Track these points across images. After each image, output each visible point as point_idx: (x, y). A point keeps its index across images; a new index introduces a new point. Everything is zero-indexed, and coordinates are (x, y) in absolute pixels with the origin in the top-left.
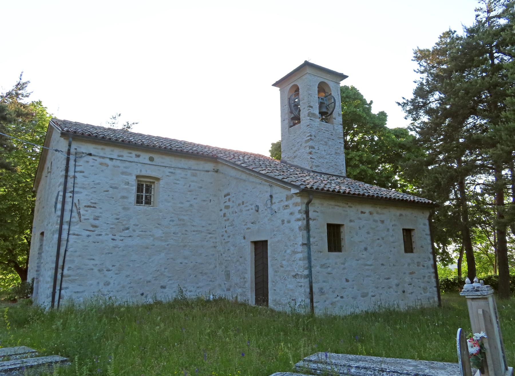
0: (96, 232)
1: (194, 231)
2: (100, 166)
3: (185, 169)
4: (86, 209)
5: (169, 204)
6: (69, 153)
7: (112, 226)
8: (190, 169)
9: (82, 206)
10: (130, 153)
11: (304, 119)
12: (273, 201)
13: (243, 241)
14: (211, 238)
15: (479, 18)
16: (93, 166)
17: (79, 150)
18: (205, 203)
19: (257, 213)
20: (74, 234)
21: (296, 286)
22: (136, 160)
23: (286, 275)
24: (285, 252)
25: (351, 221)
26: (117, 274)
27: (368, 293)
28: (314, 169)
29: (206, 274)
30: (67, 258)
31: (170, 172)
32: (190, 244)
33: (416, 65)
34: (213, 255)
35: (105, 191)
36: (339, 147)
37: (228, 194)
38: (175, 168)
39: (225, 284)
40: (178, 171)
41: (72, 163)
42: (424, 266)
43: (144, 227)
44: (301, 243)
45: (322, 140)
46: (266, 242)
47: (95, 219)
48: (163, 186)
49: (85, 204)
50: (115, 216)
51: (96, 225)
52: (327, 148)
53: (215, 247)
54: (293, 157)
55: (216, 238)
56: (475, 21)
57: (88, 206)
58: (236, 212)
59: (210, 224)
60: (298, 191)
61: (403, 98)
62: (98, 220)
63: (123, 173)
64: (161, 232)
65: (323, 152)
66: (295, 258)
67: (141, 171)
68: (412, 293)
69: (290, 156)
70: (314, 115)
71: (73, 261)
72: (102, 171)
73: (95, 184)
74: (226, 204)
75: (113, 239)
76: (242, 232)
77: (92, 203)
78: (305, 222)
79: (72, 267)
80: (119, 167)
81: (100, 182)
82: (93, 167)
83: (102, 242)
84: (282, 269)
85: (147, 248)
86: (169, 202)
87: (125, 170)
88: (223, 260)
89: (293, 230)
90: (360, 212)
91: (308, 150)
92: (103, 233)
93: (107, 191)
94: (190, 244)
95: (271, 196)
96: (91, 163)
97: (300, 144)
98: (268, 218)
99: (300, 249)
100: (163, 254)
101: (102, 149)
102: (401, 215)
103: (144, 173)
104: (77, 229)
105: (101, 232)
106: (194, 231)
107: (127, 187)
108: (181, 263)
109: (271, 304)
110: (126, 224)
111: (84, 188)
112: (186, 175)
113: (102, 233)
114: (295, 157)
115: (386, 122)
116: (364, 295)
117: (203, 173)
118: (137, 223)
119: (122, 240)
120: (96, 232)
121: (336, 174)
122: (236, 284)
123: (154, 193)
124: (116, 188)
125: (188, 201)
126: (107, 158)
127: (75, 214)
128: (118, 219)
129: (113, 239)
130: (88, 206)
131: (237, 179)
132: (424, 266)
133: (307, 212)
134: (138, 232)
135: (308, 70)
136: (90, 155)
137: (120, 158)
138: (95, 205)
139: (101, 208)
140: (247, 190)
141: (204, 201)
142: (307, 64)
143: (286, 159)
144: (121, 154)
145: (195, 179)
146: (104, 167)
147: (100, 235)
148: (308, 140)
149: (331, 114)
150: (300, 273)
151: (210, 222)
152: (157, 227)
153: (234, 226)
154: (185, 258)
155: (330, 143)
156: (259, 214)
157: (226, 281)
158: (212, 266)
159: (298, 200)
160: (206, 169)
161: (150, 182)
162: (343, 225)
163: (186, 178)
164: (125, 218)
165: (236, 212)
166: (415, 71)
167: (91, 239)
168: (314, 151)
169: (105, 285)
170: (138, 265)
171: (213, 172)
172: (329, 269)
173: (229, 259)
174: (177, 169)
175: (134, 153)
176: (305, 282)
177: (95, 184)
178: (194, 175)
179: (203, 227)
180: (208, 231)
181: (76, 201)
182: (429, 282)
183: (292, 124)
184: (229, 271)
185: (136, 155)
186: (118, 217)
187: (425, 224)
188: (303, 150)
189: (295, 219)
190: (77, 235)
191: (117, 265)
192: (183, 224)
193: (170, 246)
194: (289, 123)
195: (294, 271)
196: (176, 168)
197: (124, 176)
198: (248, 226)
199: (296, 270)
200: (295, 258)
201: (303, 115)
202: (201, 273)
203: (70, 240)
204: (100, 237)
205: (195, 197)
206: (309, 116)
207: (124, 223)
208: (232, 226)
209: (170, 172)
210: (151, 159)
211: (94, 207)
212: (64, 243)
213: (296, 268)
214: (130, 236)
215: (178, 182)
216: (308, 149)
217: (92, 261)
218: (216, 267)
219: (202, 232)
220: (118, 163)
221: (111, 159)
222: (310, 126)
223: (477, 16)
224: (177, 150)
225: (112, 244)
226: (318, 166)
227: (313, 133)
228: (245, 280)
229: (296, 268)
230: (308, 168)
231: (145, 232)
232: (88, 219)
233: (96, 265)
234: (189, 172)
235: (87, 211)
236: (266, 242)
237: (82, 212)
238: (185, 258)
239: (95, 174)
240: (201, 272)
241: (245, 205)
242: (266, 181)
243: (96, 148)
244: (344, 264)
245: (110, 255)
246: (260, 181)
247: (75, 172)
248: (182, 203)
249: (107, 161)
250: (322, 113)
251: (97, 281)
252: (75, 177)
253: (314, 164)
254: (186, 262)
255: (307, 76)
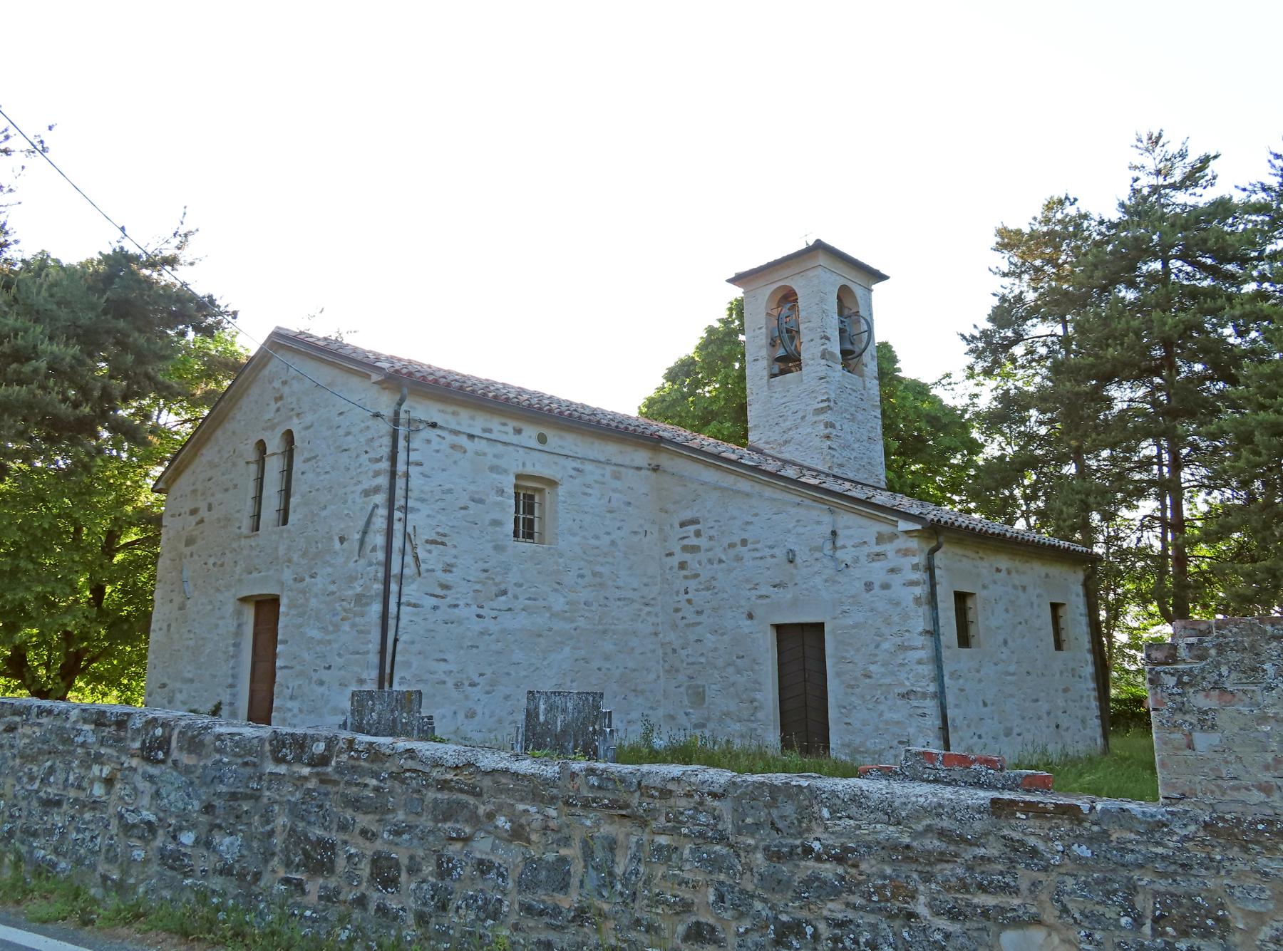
0: (448, 600)
1: (619, 599)
2: (451, 450)
3: (600, 462)
4: (429, 547)
5: (577, 539)
6: (396, 421)
7: (478, 587)
8: (608, 463)
9: (419, 541)
10: (504, 424)
11: (810, 362)
12: (839, 543)
13: (749, 622)
14: (649, 613)
15: (1137, 185)
16: (438, 451)
17: (413, 415)
18: (636, 538)
19: (789, 566)
20: (409, 604)
21: (911, 716)
22: (514, 439)
23: (879, 692)
24: (877, 646)
25: (984, 587)
26: (488, 693)
27: (1011, 729)
28: (836, 471)
29: (642, 692)
30: (398, 658)
31: (574, 469)
32: (613, 627)
33: (1002, 261)
34: (654, 651)
35: (462, 508)
36: (874, 425)
37: (694, 521)
38: (583, 459)
39: (687, 714)
40: (589, 467)
41: (402, 443)
42: (1080, 677)
43: (534, 589)
44: (920, 629)
45: (846, 410)
46: (820, 626)
47: (445, 571)
48: (563, 499)
49: (426, 537)
50: (481, 565)
51: (448, 583)
52: (855, 427)
53: (656, 634)
54: (781, 441)
55: (656, 615)
56: (1129, 191)
57: (433, 542)
58: (721, 561)
59: (645, 585)
60: (919, 527)
61: (975, 326)
62: (450, 571)
63: (493, 469)
64: (562, 600)
65: (849, 437)
66: (904, 659)
67: (524, 464)
68: (1068, 728)
69: (772, 439)
70: (832, 355)
71: (408, 664)
72: (455, 462)
73: (443, 492)
74: (686, 542)
75: (479, 616)
76: (743, 602)
77: (438, 533)
78: (926, 588)
79: (408, 678)
80: (485, 454)
81: (453, 487)
82: (439, 455)
83: (460, 623)
84: (868, 681)
85: (540, 636)
86: (574, 534)
87: (496, 462)
88: (682, 661)
89: (898, 604)
90: (994, 570)
91: (821, 429)
92: (461, 603)
93: (465, 508)
94: (613, 627)
95: (834, 533)
96: (435, 446)
97: (800, 414)
98: (824, 577)
99: (920, 641)
100: (567, 649)
101: (454, 413)
102: (1047, 576)
103: (529, 470)
104: (413, 593)
105: (458, 599)
106: (619, 599)
107: (500, 498)
108: (599, 669)
109: (833, 754)
110: (500, 583)
111: (423, 500)
112: (603, 475)
113: (459, 603)
114: (786, 442)
115: (897, 366)
116: (1008, 733)
117: (631, 472)
118: (521, 581)
119: (495, 618)
120: (448, 600)
121: (870, 482)
122: (727, 714)
123: (543, 511)
124: (481, 501)
125: (608, 533)
126: (464, 433)
127: (409, 559)
128: (486, 571)
129: (479, 616)
130: (433, 542)
131: (716, 488)
132: (1080, 677)
133: (930, 569)
134: (522, 602)
135: (822, 260)
136: (434, 425)
137: (487, 435)
138: (444, 540)
139: (455, 547)
140: (756, 515)
141: (635, 533)
142: (820, 248)
143: (761, 445)
144: (489, 425)
145: (617, 484)
146: (458, 455)
147: (456, 606)
148: (822, 408)
149: (861, 355)
150: (919, 689)
151: (645, 580)
152: (555, 590)
153: (716, 591)
154: (607, 658)
155: (859, 417)
156: (796, 567)
157: (692, 708)
158: (652, 676)
159: (914, 544)
160: (636, 464)
161: (536, 489)
162: (972, 594)
163: (603, 483)
164: (498, 569)
165: (721, 561)
166: (990, 270)
167: (440, 615)
168: (834, 432)
169: (466, 716)
170: (525, 673)
171: (649, 469)
172: (961, 681)
173: (703, 660)
174: (586, 463)
175: (512, 424)
176: (931, 706)
177: (443, 492)
178: (617, 477)
179: (635, 590)
180: (643, 601)
181: (410, 529)
182: (1088, 708)
183: (776, 370)
184: (704, 686)
185: (514, 429)
186: (486, 566)
187: (1078, 595)
188: (809, 430)
189: (903, 582)
190: (415, 606)
191: (488, 672)
192: (600, 584)
193: (578, 631)
194: (771, 368)
195: (902, 685)
196: (585, 459)
197: (494, 476)
198: (763, 591)
199: (907, 683)
200: (904, 659)
201: (809, 350)
202: (634, 691)
203: (402, 616)
204: (456, 610)
205: (619, 524)
206: (823, 357)
207: (497, 581)
208: (708, 589)
209: (574, 469)
210: (542, 439)
211: (443, 544)
212: (392, 623)
213: (908, 679)
214: (510, 609)
215: (589, 491)
216: (822, 427)
217: (442, 664)
218: (659, 677)
219: (633, 601)
220: (481, 445)
221: (471, 437)
222: (828, 379)
223: (1136, 180)
224: (608, 425)
225: (477, 626)
226: (841, 465)
227: (833, 396)
228: (755, 704)
229: (908, 679)
230: (826, 470)
231: (535, 600)
232: (433, 570)
233: (451, 672)
234: (609, 469)
235: (430, 552)
236: (820, 626)
237: (422, 554)
238: (607, 658)
239: (443, 470)
240: (633, 688)
241: (750, 546)
242: (815, 500)
243: (443, 411)
244: (978, 671)
245: (475, 650)
246: (798, 499)
247: (408, 463)
248: (597, 537)
249: (463, 440)
250: (845, 353)
251: (454, 708)
252: (407, 475)
253: (835, 460)
254: (608, 666)
255: (819, 271)
